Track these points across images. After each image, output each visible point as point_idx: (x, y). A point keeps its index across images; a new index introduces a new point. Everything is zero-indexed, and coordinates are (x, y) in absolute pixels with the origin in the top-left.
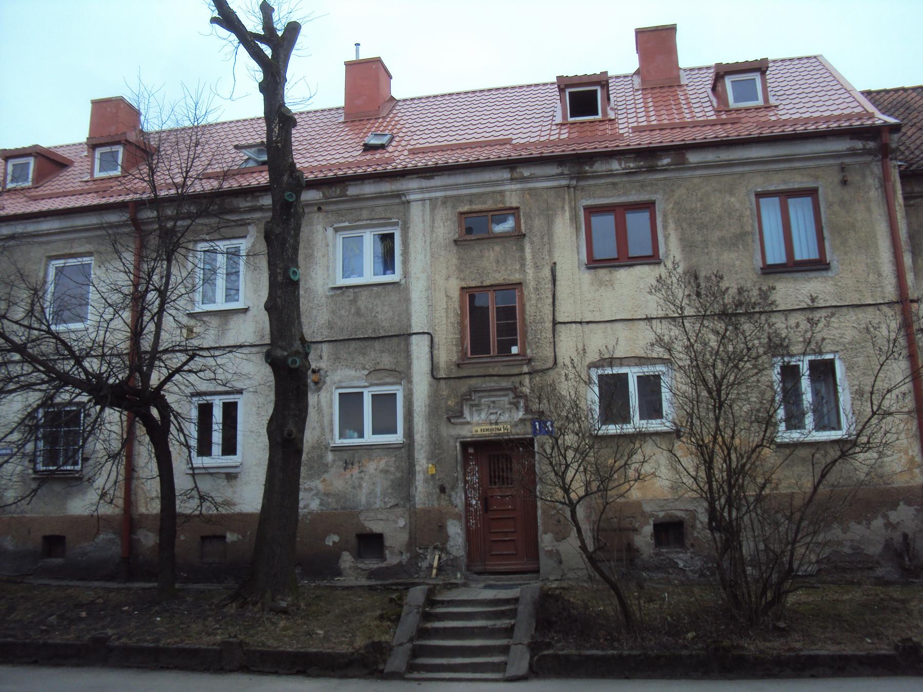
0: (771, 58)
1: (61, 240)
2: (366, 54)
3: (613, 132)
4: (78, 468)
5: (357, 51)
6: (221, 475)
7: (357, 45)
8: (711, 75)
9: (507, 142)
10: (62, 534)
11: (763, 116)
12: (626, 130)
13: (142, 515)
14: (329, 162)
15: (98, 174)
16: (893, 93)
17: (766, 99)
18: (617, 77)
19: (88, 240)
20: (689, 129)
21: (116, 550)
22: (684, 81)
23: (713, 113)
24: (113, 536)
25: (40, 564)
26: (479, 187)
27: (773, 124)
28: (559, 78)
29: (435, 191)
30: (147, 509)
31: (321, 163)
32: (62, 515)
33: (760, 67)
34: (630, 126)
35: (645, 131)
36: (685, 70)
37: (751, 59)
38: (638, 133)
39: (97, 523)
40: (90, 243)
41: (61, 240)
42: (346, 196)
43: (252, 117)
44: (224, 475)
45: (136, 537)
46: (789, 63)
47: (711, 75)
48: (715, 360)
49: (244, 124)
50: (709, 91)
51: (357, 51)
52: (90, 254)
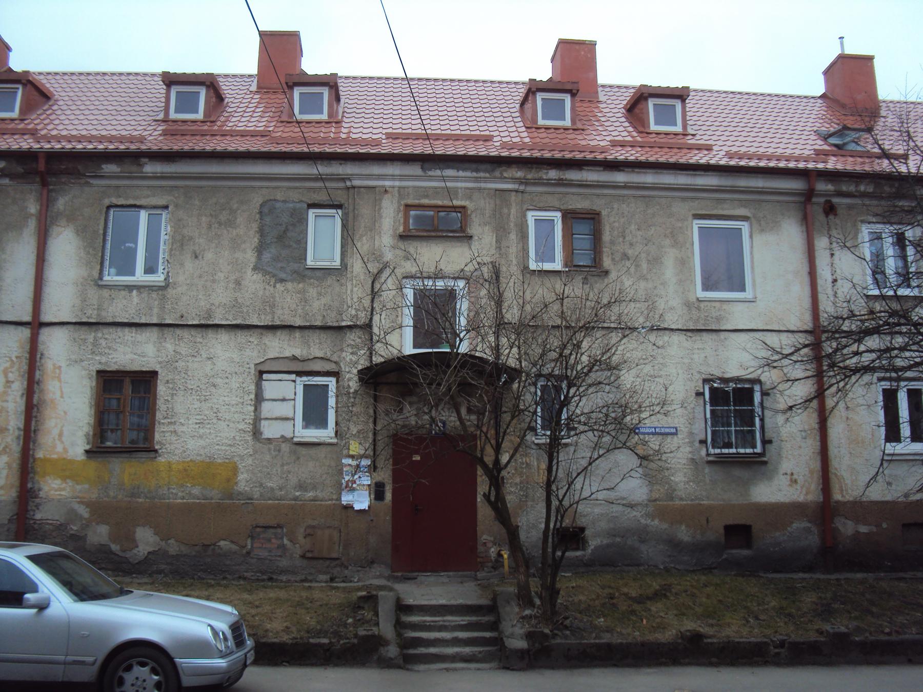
0: (692, 87)
1: (709, 199)
2: (852, 49)
3: (337, 135)
4: (759, 449)
5: (842, 44)
6: (918, 462)
7: (841, 38)
8: (521, 94)
9: (488, 139)
10: (748, 523)
11: (322, 132)
12: (380, 135)
13: (837, 502)
14: (90, 132)
15: (173, 115)
16: (562, 131)
17: (685, 126)
18: (347, 78)
19: (743, 204)
20: (462, 142)
21: (813, 540)
22: (602, 97)
23: (524, 129)
24: (809, 525)
25: (725, 556)
26: (465, 181)
27: (337, 141)
28: (530, 80)
29: (461, 181)
30: (843, 496)
31: (130, 132)
32: (745, 502)
33: (681, 95)
34: (384, 131)
35: (418, 139)
36: (603, 86)
37: (673, 85)
38: (391, 140)
39: (796, 509)
40: (745, 207)
41: (709, 199)
42: (142, 172)
43: (40, 70)
44: (921, 462)
45: (833, 525)
46: (513, 86)
47: (521, 94)
48: (834, 384)
49: (48, 77)
50: (518, 106)
51: (842, 44)
52: (745, 218)
